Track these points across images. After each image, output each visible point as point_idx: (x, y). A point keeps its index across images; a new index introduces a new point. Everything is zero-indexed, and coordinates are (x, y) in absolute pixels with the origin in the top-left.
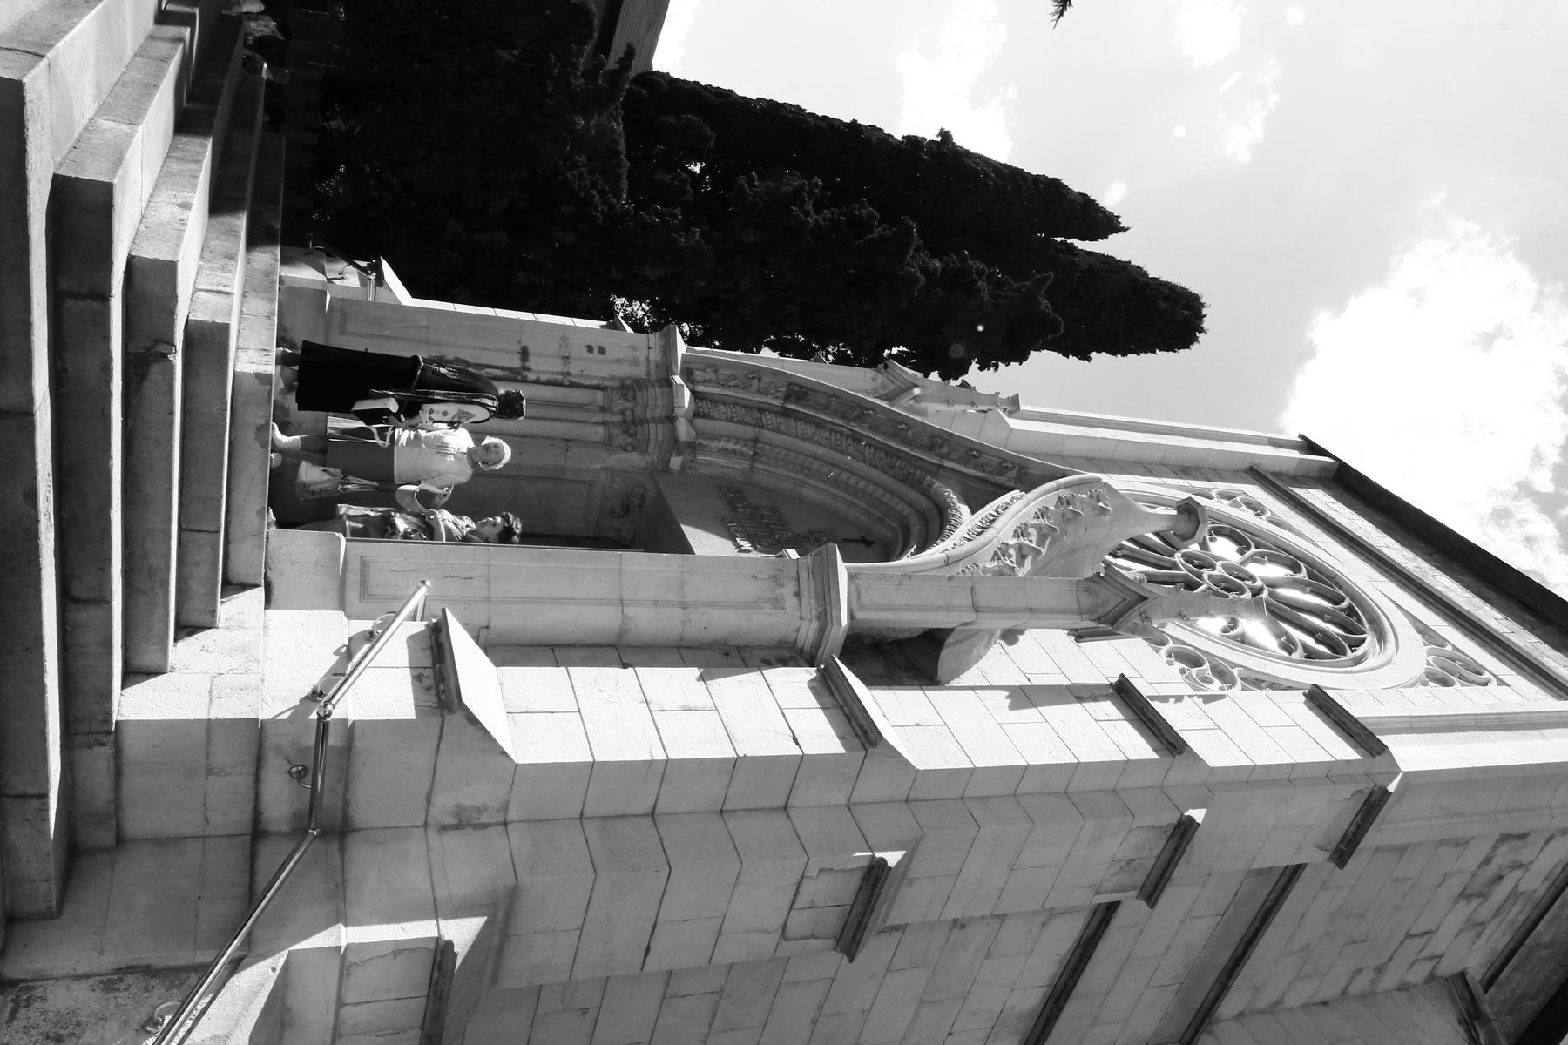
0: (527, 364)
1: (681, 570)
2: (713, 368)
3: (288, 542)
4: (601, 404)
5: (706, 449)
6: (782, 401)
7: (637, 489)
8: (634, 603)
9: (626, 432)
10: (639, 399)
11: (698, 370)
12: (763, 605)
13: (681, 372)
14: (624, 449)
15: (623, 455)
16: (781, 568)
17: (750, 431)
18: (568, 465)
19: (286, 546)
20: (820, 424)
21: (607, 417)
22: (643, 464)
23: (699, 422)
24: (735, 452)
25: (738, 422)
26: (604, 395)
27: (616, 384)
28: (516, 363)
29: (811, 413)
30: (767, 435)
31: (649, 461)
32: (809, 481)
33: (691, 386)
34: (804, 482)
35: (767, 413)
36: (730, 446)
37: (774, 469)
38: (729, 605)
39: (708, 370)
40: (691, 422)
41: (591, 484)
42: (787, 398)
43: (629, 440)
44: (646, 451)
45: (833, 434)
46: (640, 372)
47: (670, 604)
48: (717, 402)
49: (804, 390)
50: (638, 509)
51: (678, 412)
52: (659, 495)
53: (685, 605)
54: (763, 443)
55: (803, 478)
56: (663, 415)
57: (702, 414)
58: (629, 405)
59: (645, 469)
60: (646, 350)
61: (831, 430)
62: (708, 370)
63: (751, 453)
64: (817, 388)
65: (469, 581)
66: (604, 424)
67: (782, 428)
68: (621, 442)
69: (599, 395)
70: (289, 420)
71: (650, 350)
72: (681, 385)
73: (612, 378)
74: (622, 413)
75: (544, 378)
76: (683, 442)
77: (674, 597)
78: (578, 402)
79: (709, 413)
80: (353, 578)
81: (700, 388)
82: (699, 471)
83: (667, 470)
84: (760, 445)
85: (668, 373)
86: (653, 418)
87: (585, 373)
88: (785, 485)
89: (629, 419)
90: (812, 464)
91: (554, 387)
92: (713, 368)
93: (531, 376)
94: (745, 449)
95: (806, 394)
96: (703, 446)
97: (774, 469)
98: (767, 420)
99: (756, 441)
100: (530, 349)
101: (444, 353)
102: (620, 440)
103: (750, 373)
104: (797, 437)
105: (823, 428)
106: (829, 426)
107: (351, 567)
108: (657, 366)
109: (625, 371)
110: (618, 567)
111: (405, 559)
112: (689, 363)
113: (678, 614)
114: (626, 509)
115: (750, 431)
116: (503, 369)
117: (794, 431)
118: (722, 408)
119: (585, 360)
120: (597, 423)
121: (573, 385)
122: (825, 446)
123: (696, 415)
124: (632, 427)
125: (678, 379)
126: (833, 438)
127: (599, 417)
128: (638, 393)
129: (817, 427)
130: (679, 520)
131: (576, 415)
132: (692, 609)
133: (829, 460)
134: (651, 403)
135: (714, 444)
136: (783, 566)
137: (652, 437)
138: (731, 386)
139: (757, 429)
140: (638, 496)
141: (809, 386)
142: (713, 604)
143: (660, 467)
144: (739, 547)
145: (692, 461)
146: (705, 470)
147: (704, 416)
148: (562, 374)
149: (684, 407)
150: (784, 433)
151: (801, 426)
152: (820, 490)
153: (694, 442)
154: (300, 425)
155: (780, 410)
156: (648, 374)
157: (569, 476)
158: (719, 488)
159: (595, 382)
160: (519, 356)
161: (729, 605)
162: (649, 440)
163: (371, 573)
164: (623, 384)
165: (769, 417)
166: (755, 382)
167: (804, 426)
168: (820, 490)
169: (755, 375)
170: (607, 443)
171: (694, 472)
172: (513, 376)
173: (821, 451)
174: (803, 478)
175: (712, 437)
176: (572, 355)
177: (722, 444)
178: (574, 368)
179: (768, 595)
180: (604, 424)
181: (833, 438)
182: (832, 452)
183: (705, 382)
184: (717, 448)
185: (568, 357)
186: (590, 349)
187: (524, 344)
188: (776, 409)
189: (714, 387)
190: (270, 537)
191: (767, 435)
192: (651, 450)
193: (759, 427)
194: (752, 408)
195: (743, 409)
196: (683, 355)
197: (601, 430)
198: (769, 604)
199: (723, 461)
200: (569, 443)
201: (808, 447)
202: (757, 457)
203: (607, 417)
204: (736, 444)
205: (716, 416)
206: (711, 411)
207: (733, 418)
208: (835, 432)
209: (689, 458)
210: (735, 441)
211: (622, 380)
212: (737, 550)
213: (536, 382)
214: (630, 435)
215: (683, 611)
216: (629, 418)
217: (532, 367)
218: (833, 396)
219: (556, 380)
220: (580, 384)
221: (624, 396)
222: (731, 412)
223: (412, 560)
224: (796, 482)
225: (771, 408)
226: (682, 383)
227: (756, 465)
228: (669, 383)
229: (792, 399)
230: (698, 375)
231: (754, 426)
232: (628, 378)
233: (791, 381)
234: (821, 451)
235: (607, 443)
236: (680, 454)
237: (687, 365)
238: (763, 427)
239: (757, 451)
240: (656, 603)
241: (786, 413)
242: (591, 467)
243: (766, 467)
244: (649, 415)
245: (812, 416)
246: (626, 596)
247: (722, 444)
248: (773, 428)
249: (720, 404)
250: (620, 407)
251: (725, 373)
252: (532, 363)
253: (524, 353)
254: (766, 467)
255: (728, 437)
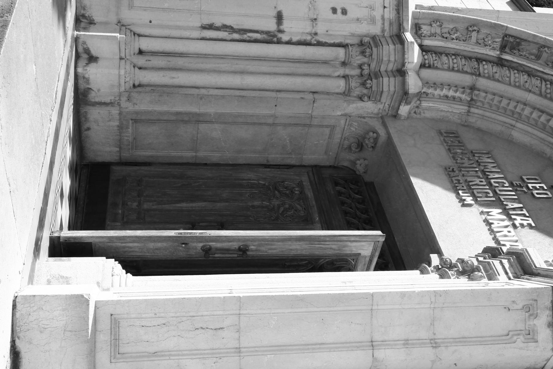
0: (282, 27)
1: (432, 306)
2: (438, 23)
3: (35, 308)
4: (343, 60)
5: (429, 96)
6: (498, 53)
7: (371, 134)
8: (385, 344)
9: (363, 84)
10: (375, 56)
11: (424, 24)
12: (515, 338)
13: (412, 28)
14: (361, 98)
15: (360, 104)
16: (536, 298)
17: (467, 80)
18: (314, 114)
19: (34, 311)
20: (531, 73)
21: (348, 71)
22: (376, 111)
23: (426, 73)
24: (454, 98)
25: (458, 71)
26: (346, 52)
27: (356, 41)
28: (271, 26)
29: (525, 63)
30: (482, 83)
31: (382, 108)
32: (519, 125)
33: (419, 41)
34: (514, 126)
35: (484, 63)
36: (451, 93)
37: (487, 114)
38: (481, 341)
39: (434, 25)
40: (418, 74)
41: (333, 128)
42: (503, 48)
43: (365, 91)
44: (380, 101)
45: (544, 83)
46: (376, 30)
47: (421, 343)
48: (441, 54)
49: (518, 40)
50: (371, 149)
51: (408, 66)
52: (389, 138)
53: (436, 343)
54: (479, 90)
55: (513, 123)
56: (395, 69)
57: (427, 65)
58: (365, 60)
59: (378, 114)
60: (382, 9)
61: (542, 79)
62: (434, 25)
63: (469, 99)
64: (530, 39)
65: (221, 331)
66: (345, 77)
67: (497, 76)
68: (358, 93)
69: (341, 52)
70: (90, 87)
71: (385, 9)
72: (412, 42)
73: (353, 35)
74: (360, 66)
75: (295, 39)
76: (412, 94)
77: (424, 334)
78: (324, 59)
79: (433, 64)
80: (103, 338)
81: (427, 42)
82: (422, 114)
83: (396, 116)
84: (476, 92)
85: (400, 30)
86: (386, 71)
87: (330, 32)
88: (498, 128)
89: (366, 73)
90: (523, 110)
91: (305, 47)
92: (438, 23)
93: (285, 38)
94: (463, 96)
95: (519, 44)
96: (427, 94)
97: (487, 114)
98: (484, 69)
99: (473, 88)
100: (285, 14)
101: (214, 22)
102: (358, 91)
103: (471, 26)
104: (510, 84)
105: (534, 76)
106: (540, 74)
107: (100, 327)
108: (391, 24)
109: (364, 29)
110: (370, 308)
111: (155, 314)
112: (418, 19)
113: (429, 352)
114: (361, 146)
115: (467, 80)
116: (261, 32)
117: (508, 79)
118: (444, 58)
119: (330, 21)
120: (339, 76)
121: (320, 44)
122: (534, 93)
123: (423, 66)
124: (369, 82)
125: (409, 36)
126: (543, 86)
127: (341, 71)
128: (375, 50)
129: (529, 75)
130: (409, 170)
131: (323, 70)
132: (443, 348)
133: (538, 106)
134: (385, 59)
135: (437, 92)
136: (538, 296)
137: (385, 89)
138: (453, 39)
139: (474, 77)
140: (372, 141)
141: (523, 37)
142: (463, 341)
143: (390, 113)
144: (462, 201)
145: (417, 107)
146: (428, 115)
147: (429, 67)
148: (310, 34)
149: (413, 63)
150: (498, 81)
151: (514, 76)
152: (527, 133)
153: (420, 92)
154: (99, 90)
155: (495, 60)
156: (383, 31)
157: (315, 122)
158: (440, 133)
159: (337, 41)
160: (274, 21)
161: (481, 341)
162: (382, 92)
163: (121, 330)
164: (361, 41)
165: (486, 67)
166: (474, 34)
167: (517, 75)
168: (527, 133)
169: (475, 28)
170: (346, 94)
171: (418, 116)
172: (269, 38)
173: (531, 98)
174: (513, 123)
175: (435, 85)
176: (319, 17)
177: (445, 92)
178: (321, 28)
179: (521, 326)
180: (345, 77)
181: (543, 86)
182: (540, 98)
183: (432, 35)
184: (440, 95)
185: (315, 19)
186: (334, 10)
187: (279, 10)
188: (491, 59)
189: (439, 40)
190: (17, 304)
191: (482, 83)
192: (383, 100)
193: (476, 75)
194: (470, 58)
195: (463, 60)
196: (413, 12)
197: (342, 83)
198: (521, 337)
199: (443, 106)
200: (316, 96)
201: (519, 94)
202: (473, 102)
203: (348, 71)
204: (456, 91)
205: (439, 66)
206: (436, 62)
207: (453, 67)
208: (546, 81)
209: (415, 105)
210: (455, 89)
211: (362, 36)
212: (460, 204)
213: (289, 43)
214: (367, 88)
215: (434, 351)
216: (366, 72)
217: (285, 30)
218: (544, 46)
219: (305, 40)
220: (326, 43)
221: (363, 53)
222: (454, 63)
223: (162, 315)
224: (507, 125)
225: (488, 58)
226: (413, 40)
227: (472, 110)
228: (399, 39)
229: (507, 50)
230: (425, 29)
231: (472, 74)
232: (365, 36)
233: (507, 32)
234: (531, 98)
235: (346, 94)
236: (407, 103)
237: (416, 21)
238: (479, 75)
239: (475, 98)
240: (407, 343)
241: (500, 63)
242: (333, 114)
243: (480, 112)
244: (383, 69)
245: (524, 65)
246: (377, 337)
247: (445, 92)
248: (482, 62)
249: (443, 55)
250: (359, 62)
251: (448, 26)
252: (286, 26)
253: (279, 17)
254: (480, 112)
255: (449, 85)
